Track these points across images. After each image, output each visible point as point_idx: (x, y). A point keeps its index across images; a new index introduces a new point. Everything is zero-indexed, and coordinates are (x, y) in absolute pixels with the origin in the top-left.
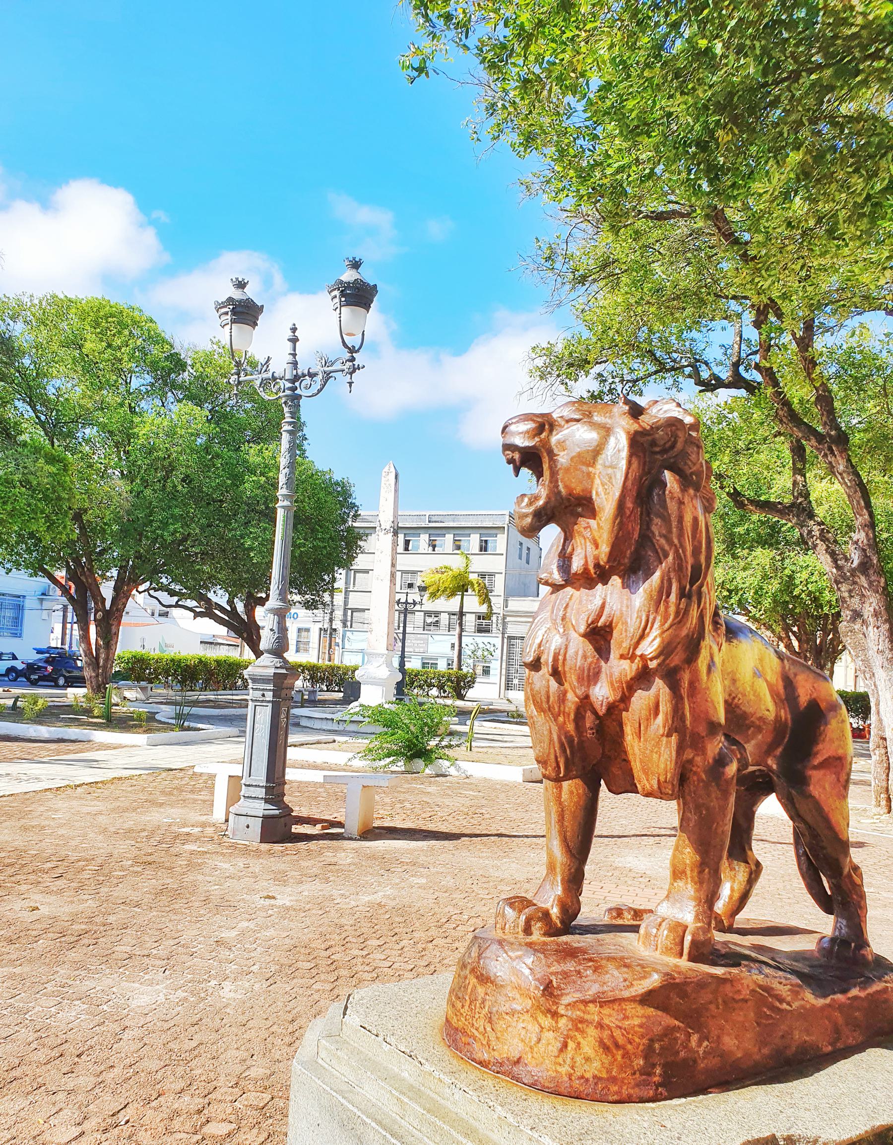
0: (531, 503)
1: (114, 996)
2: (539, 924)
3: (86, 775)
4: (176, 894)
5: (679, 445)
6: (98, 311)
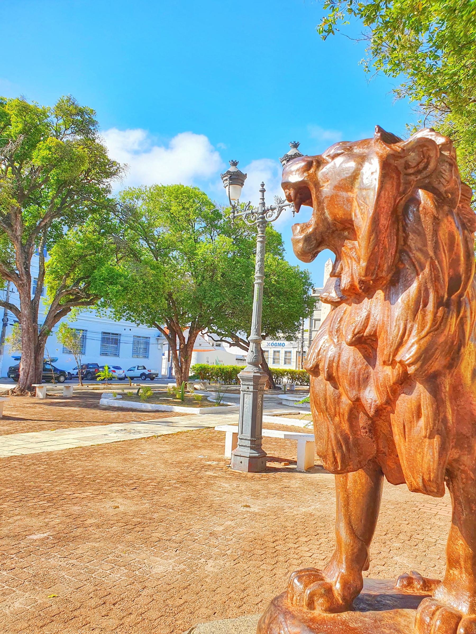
0: (302, 230)
1: (144, 565)
2: (321, 600)
3: (165, 430)
4: (194, 502)
5: (432, 166)
6: (178, 191)
